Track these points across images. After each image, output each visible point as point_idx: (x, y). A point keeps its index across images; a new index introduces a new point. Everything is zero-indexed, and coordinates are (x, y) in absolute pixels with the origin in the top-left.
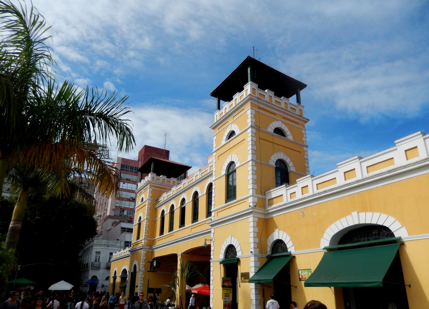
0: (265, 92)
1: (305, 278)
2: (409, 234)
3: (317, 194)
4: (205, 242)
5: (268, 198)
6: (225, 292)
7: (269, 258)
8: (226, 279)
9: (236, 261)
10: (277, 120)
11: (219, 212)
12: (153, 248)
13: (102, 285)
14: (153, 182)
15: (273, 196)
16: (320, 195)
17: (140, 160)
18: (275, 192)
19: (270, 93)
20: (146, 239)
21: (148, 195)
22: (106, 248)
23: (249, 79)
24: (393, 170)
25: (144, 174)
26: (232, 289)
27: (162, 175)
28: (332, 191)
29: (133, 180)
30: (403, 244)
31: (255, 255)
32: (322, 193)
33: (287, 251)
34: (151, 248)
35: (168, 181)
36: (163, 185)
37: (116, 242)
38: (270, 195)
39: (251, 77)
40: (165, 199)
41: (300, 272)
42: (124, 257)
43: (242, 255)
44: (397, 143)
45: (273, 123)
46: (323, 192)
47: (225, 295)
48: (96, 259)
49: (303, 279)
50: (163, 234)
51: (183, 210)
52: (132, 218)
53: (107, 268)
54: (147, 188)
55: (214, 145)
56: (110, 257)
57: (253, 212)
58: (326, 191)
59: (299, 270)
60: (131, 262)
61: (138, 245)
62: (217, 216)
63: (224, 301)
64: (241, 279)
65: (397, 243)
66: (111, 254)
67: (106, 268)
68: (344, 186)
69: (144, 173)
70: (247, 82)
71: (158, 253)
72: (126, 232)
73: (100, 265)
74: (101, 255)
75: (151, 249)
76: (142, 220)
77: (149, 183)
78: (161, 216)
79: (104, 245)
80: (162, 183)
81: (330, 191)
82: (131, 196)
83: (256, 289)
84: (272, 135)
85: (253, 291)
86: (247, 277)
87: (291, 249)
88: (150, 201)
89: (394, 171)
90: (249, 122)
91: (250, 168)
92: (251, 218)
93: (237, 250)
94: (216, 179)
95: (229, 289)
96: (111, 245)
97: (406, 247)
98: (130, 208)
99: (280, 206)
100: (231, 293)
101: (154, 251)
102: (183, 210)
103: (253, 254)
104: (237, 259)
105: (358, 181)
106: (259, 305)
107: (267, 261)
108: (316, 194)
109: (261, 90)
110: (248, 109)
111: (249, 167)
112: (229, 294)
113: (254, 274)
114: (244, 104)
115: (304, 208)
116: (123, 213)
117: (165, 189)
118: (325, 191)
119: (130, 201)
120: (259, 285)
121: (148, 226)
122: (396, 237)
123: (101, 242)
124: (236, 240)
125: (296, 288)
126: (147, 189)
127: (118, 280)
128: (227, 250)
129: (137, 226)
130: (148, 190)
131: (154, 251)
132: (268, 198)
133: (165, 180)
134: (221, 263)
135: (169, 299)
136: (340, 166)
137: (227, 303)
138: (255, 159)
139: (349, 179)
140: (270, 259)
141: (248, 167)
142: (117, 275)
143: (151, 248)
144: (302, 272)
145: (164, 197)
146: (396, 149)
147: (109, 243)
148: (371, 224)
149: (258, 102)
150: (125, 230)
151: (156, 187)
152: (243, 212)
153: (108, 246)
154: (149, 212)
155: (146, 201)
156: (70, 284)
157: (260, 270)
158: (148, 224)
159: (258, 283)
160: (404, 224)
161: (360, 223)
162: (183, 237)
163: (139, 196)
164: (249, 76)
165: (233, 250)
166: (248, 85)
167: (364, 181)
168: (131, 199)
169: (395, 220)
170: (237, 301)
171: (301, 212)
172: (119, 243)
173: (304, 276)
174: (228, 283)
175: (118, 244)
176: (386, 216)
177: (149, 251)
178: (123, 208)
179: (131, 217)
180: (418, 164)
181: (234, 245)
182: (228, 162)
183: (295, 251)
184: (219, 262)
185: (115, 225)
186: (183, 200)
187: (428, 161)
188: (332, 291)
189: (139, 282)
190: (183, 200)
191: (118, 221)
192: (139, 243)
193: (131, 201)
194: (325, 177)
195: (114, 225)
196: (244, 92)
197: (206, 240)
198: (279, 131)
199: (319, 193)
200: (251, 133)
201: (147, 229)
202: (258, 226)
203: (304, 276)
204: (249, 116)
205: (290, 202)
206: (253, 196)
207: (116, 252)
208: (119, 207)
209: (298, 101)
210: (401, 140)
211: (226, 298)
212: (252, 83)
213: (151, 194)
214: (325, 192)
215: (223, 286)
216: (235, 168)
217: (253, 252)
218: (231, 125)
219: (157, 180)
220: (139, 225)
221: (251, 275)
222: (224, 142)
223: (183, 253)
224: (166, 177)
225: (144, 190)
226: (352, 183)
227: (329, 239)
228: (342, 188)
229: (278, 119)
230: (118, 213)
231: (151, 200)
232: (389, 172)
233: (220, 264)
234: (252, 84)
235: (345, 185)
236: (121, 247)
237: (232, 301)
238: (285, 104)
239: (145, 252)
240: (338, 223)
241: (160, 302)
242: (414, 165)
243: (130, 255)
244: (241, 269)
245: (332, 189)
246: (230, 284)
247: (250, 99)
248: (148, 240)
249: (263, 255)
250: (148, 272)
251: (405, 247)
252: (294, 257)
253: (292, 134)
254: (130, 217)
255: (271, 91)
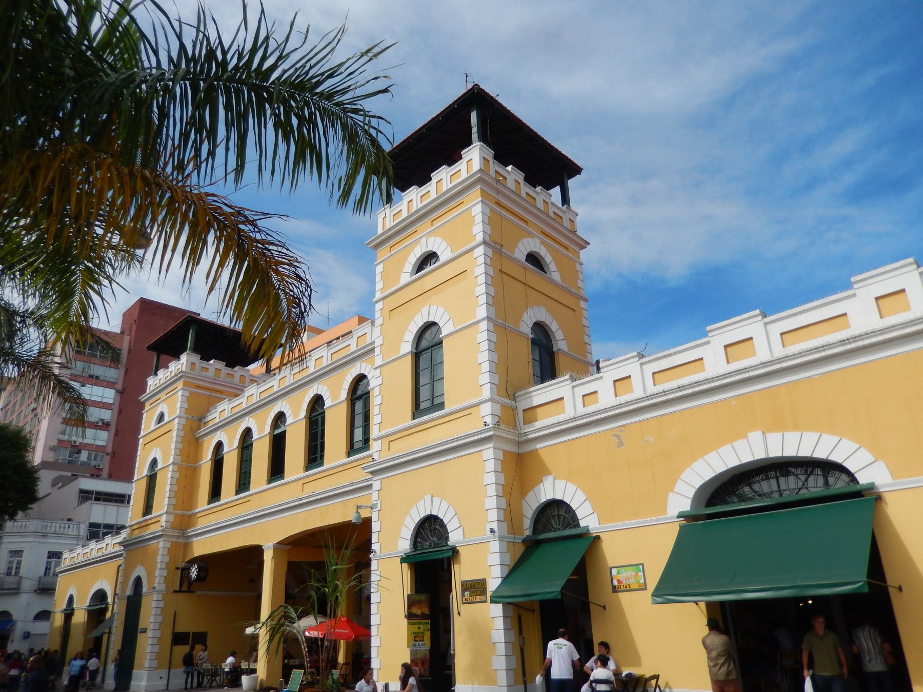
0: (507, 171)
1: (629, 585)
2: (892, 477)
3: (661, 393)
4: (357, 512)
5: (523, 405)
6: (415, 628)
7: (528, 545)
8: (417, 598)
9: (450, 554)
10: (531, 235)
11: (392, 441)
12: (190, 534)
13: (25, 633)
14: (191, 374)
15: (537, 399)
16: (665, 395)
17: (127, 332)
18: (542, 394)
19: (517, 173)
20: (171, 514)
21: (178, 405)
22: (37, 540)
23: (475, 136)
24: (854, 339)
25: (164, 357)
26: (429, 621)
27: (215, 359)
28: (699, 385)
29: (108, 379)
30: (879, 498)
31: (501, 538)
32: (673, 391)
33: (578, 525)
34: (185, 535)
35: (227, 373)
36: (216, 382)
37: (67, 526)
38: (527, 400)
39: (478, 132)
40: (226, 416)
41: (614, 571)
42: (112, 557)
43: (464, 539)
44: (857, 282)
45: (525, 241)
46: (674, 389)
47: (415, 637)
48: (10, 569)
49: (622, 588)
50: (220, 498)
51: (278, 443)
52: (101, 467)
53: (38, 589)
54: (176, 388)
55: (379, 286)
56: (47, 562)
57: (493, 438)
58: (682, 387)
59: (611, 568)
60: (122, 573)
61: (148, 529)
62: (389, 450)
63: (411, 651)
64: (463, 596)
65: (863, 496)
66: (55, 555)
67: (35, 591)
68: (729, 375)
69: (162, 354)
70: (469, 143)
71: (202, 547)
72: (93, 501)
73: (19, 583)
74: (25, 559)
75: (184, 536)
76: (160, 466)
77: (182, 377)
78: (212, 456)
79: (34, 532)
80: (215, 379)
81: (692, 385)
82: (100, 415)
83: (505, 617)
84: (524, 268)
85: (499, 623)
86: (480, 591)
87: (588, 519)
88: (183, 421)
89: (854, 342)
90: (478, 231)
91: (484, 336)
92: (488, 453)
93: (449, 528)
94: (382, 365)
95: (424, 621)
96: (53, 532)
97: (886, 504)
98: (96, 445)
99: (559, 423)
100: (427, 630)
101: (192, 542)
102: (278, 443)
103: (495, 535)
104: (451, 549)
105: (766, 363)
106: (511, 654)
107: (524, 552)
108: (657, 394)
109: (500, 164)
110: (474, 203)
111: (482, 334)
112: (423, 633)
113: (499, 581)
114: (465, 189)
115: (622, 426)
116: (79, 458)
117: (221, 392)
118: (679, 388)
119: (96, 429)
120: (511, 606)
121: (177, 482)
122: (861, 483)
123: (26, 526)
124: (445, 504)
125: (605, 609)
126: (177, 392)
127: (80, 617)
128: (418, 529)
129: (143, 484)
130: (180, 393)
131: (190, 540)
132: (523, 405)
133: (222, 372)
134: (403, 560)
135: (232, 655)
136: (715, 333)
137: (420, 655)
138: (493, 316)
139: (737, 359)
140: (532, 546)
141: (478, 335)
142: (75, 606)
143: (185, 535)
144: (618, 573)
145: (223, 410)
146: (854, 295)
147: (46, 528)
148: (782, 457)
149: (498, 191)
150: (90, 495)
151: (198, 387)
152: (466, 438)
153: (45, 535)
154: (180, 446)
155: (174, 419)
156: (589, 595)
157: (512, 573)
158: (177, 475)
159: (509, 603)
160: (879, 453)
161: (768, 455)
162: (280, 505)
163: (152, 408)
164: (474, 130)
165: (435, 529)
166: (472, 150)
167: (780, 363)
168: (100, 424)
169: (858, 446)
170: (452, 649)
171: (613, 435)
172: (73, 528)
173: (626, 581)
174: (420, 608)
175: (71, 530)
176: (836, 439)
177: (180, 543)
178: (78, 444)
179: (99, 466)
180: (914, 325)
181: (440, 516)
182: (420, 324)
183: (598, 524)
184: (399, 560)
185: (60, 484)
186: (280, 417)
187: (920, 323)
188: (702, 610)
189: (152, 619)
190: (280, 417)
191: (69, 474)
192: (150, 522)
193: (101, 428)
194: (674, 357)
195: (58, 483)
196: (461, 165)
197: (358, 507)
198: (534, 259)
199: (664, 392)
200: (485, 258)
201: (175, 488)
202: (503, 471)
203: (626, 581)
204: (479, 218)
205: (588, 414)
206: (491, 400)
207: (73, 550)
208: (69, 441)
209: (565, 199)
210: (865, 277)
211: (417, 643)
212: (482, 146)
213: (187, 404)
214: (681, 389)
215: (410, 616)
216: (441, 336)
217: (496, 529)
218: (427, 238)
219: (201, 370)
220: (152, 479)
221: (493, 585)
222: (405, 278)
223: (279, 543)
224: (225, 363)
225: (167, 394)
226: (751, 367)
227: (691, 493)
228: (724, 379)
229: (534, 234)
230: (64, 455)
231: (187, 419)
232: (842, 343)
233: (401, 563)
234: (482, 148)
235: (732, 372)
236: (78, 537)
237: (430, 649)
238: (545, 203)
239: (168, 545)
240: (712, 457)
241: (207, 665)
242: (903, 328)
243: (123, 552)
244: (461, 573)
245: (697, 382)
246: (426, 611)
247: (480, 180)
248: (176, 515)
249: (516, 536)
250: (175, 594)
251: (884, 505)
252: (598, 538)
253: (559, 270)
254: (95, 466)
255: (518, 170)
